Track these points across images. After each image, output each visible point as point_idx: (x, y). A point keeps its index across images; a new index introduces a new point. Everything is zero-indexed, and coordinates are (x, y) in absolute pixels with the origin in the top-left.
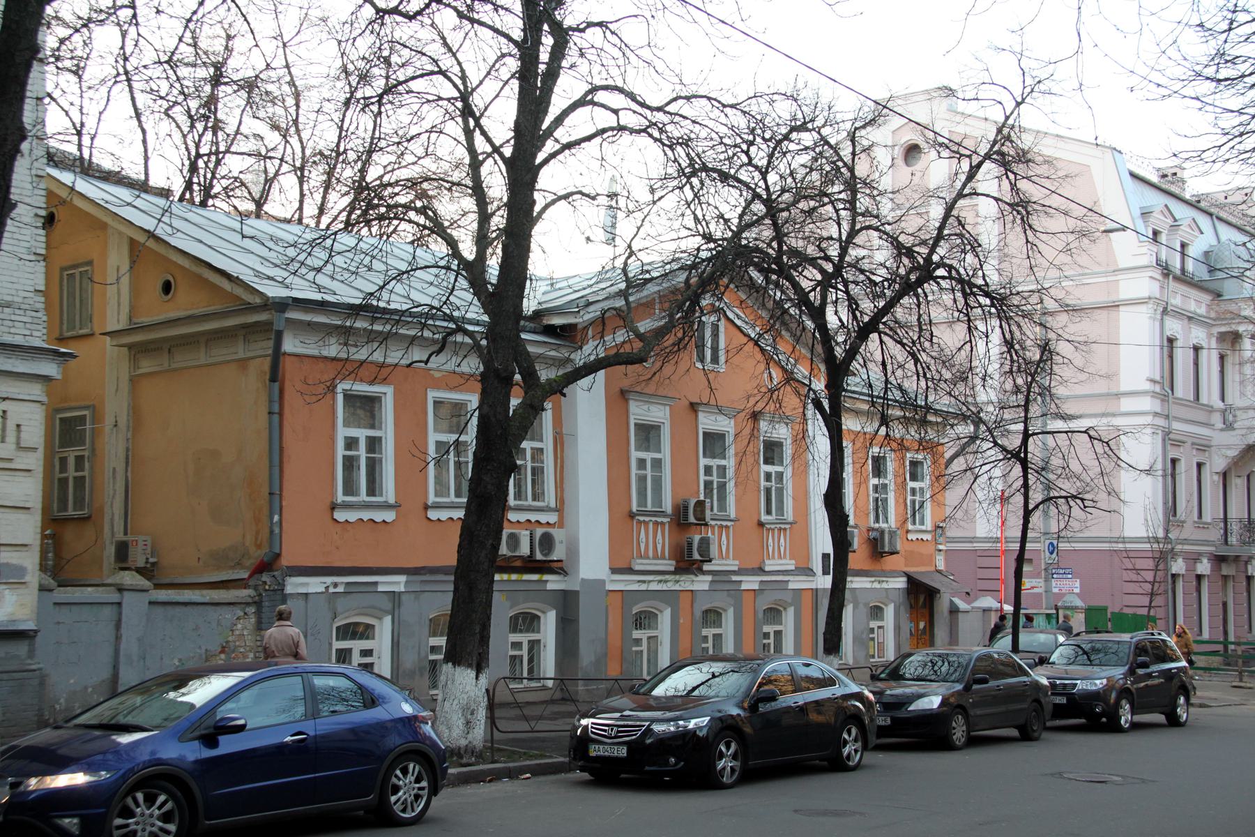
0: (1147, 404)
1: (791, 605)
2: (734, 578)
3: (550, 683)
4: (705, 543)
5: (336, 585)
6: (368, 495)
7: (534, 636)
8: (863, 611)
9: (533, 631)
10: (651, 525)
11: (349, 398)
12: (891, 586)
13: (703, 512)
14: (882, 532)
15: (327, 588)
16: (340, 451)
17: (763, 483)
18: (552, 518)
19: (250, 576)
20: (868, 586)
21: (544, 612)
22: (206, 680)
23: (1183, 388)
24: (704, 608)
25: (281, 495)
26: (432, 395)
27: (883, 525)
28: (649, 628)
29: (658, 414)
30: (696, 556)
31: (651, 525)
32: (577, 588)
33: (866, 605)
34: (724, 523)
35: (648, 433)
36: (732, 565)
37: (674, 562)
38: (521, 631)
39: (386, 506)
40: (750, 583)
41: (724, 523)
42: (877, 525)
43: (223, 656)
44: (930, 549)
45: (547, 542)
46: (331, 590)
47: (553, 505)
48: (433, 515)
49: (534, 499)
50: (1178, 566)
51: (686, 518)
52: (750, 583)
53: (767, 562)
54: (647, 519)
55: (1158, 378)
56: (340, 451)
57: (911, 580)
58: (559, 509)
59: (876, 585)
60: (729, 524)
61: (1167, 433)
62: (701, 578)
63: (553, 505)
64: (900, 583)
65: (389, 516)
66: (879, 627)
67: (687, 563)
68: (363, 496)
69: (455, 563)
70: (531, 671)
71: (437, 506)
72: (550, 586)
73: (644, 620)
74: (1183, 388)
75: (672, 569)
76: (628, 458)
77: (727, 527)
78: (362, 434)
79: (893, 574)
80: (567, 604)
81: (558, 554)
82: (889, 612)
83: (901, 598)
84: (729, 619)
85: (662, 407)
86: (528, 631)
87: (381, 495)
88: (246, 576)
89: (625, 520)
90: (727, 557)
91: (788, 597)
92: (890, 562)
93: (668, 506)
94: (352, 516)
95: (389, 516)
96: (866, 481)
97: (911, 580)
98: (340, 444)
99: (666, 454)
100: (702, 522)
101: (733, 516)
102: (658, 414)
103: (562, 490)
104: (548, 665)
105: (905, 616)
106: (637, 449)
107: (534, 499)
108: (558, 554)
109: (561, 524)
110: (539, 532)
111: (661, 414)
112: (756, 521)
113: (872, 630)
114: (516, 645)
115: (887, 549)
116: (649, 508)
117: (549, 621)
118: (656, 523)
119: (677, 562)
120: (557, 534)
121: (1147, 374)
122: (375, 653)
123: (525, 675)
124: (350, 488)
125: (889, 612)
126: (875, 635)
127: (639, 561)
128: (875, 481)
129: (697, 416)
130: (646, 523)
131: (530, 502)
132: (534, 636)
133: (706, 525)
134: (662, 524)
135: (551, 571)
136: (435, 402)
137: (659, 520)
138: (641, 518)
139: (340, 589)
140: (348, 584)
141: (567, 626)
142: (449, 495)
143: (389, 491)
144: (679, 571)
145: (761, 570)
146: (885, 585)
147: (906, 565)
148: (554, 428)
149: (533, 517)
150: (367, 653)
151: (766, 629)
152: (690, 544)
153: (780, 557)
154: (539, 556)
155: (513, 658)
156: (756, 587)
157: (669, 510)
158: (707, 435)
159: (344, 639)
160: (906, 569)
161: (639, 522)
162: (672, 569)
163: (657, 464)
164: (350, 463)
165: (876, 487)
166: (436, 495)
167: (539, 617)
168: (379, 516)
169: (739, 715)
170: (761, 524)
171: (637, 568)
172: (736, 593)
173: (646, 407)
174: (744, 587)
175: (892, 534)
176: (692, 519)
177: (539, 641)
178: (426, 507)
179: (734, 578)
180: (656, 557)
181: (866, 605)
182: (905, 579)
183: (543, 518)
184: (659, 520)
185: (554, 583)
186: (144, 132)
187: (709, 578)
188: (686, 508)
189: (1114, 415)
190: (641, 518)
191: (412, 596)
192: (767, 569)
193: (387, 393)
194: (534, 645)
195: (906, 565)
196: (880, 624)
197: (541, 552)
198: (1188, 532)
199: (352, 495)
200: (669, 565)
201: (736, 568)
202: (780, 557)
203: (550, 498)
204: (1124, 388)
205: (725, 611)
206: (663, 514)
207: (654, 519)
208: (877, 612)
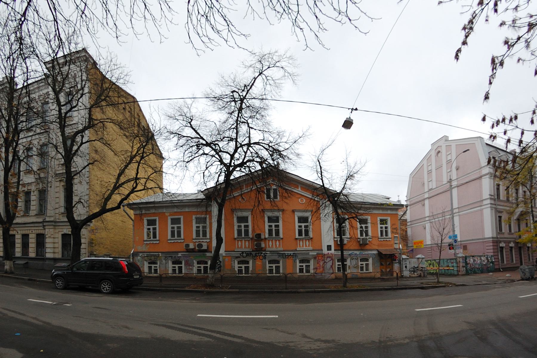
0: (489, 201)
23: (503, 196)
39: (207, 239)
44: (392, 243)
50: (502, 245)
55: (493, 194)
61: (496, 209)
71: (146, 241)
74: (503, 196)
82: (371, 261)
91: (310, 257)
95: (183, 241)
121: (489, 193)
131: (385, 237)
160: (377, 248)
164: (382, 232)
189: (482, 206)
193: (182, 217)
198: (506, 235)
203: (208, 236)
204: (484, 198)
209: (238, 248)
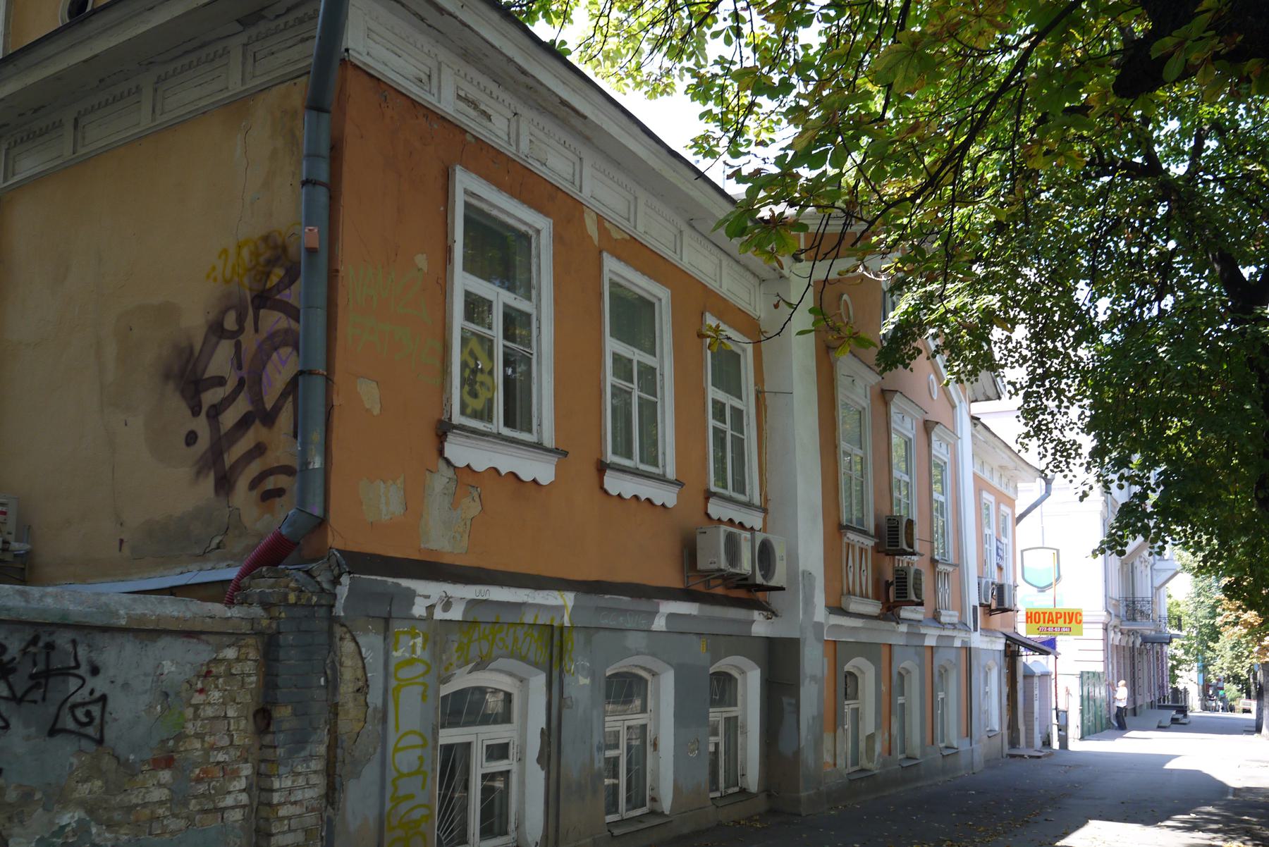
19: (246, 573)
25: (329, 379)
43: (165, 776)
46: (439, 615)
49: (616, 746)
68: (498, 425)
78: (498, 296)
88: (232, 573)
89: (837, 529)
107: (616, 746)
117: (751, 683)
122: (512, 751)
139: (456, 614)
150: (499, 751)
157: (870, 525)
169: (1125, 685)
178: (602, 467)
185: (761, 626)
186: (363, 659)
203: (754, 493)
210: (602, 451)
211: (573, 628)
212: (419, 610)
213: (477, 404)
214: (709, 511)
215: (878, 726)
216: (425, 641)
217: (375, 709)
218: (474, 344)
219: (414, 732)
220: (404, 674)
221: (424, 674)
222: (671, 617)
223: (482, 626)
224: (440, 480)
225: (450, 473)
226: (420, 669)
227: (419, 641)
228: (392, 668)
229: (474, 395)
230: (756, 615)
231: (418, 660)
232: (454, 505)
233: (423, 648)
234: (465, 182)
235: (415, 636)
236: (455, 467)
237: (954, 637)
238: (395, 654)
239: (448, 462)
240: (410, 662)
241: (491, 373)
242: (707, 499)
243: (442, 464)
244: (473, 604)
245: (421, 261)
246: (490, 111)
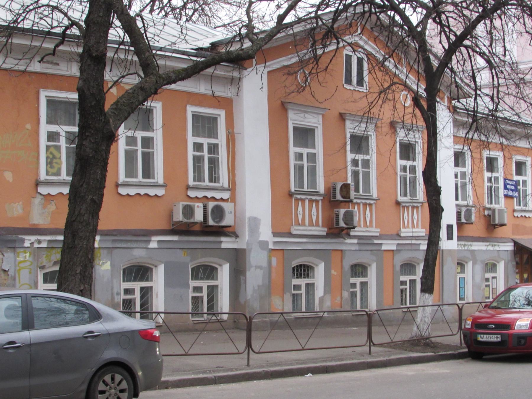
1: (470, 260)
2: (376, 241)
3: (225, 317)
4: (349, 216)
5: (39, 242)
6: (144, 177)
7: (212, 283)
8: (479, 268)
9: (412, 275)
10: (410, 208)
11: (196, 117)
12: (502, 248)
13: (348, 192)
14: (494, 211)
15: (32, 244)
16: (191, 152)
17: (399, 173)
18: (226, 195)
20: (484, 248)
21: (221, 265)
22: (98, 310)
24: (355, 261)
26: (191, 109)
27: (494, 206)
28: (308, 276)
29: (312, 120)
30: (342, 224)
31: (410, 208)
32: (244, 247)
33: (482, 262)
34: (368, 202)
35: (304, 135)
36: (374, 231)
37: (326, 229)
38: (202, 279)
39: (156, 186)
40: (389, 245)
41: (368, 202)
42: (491, 206)
45: (219, 212)
46: (36, 245)
47: (226, 185)
48: (123, 191)
51: (338, 199)
52: (389, 245)
53: (403, 230)
54: (303, 197)
56: (292, 162)
57: (516, 244)
58: (232, 188)
59: (490, 248)
60: (372, 202)
62: (349, 241)
63: (226, 185)
64: (509, 247)
65: (160, 192)
66: (493, 278)
67: (338, 230)
69: (64, 227)
70: (211, 307)
71: (126, 185)
72: (224, 246)
73: (303, 270)
75: (325, 234)
76: (288, 152)
77: (370, 205)
78: (205, 141)
79: (503, 240)
80: (238, 260)
81: (228, 220)
82: (501, 267)
83: (509, 257)
84: (372, 272)
85: (316, 116)
86: (208, 278)
87: (154, 178)
89: (284, 199)
90: (371, 226)
92: (500, 232)
93: (321, 188)
94: (132, 191)
96: (481, 172)
97: (516, 244)
98: (190, 147)
99: (319, 149)
100: (347, 200)
101: (375, 196)
102: (312, 120)
103: (234, 176)
104: (224, 303)
105: (512, 268)
106: (295, 146)
108: (228, 220)
109: (233, 199)
110: (211, 205)
111: (315, 120)
112: (394, 201)
113: (487, 280)
114: (198, 289)
115: (497, 222)
116: (306, 189)
117: (224, 273)
118: (311, 201)
119: (330, 229)
120: (227, 207)
123: (205, 310)
124: (198, 177)
125: (501, 267)
126: (490, 283)
127: (296, 228)
128: (489, 174)
129: (345, 125)
130: (303, 201)
131: (207, 183)
132: (212, 283)
133: (351, 201)
134: (317, 201)
135: (226, 235)
136: (193, 115)
137: (314, 198)
138: (299, 197)
139: (44, 245)
140: (398, 244)
141: (238, 274)
142: (136, 177)
143: (159, 176)
144: (329, 235)
145: (398, 236)
146: (497, 248)
147: (513, 233)
148: (227, 129)
149: (209, 194)
151: (403, 278)
152: (338, 216)
153: (413, 226)
154: (211, 222)
155: (402, 291)
156: (394, 248)
158: (353, 137)
159: (129, 280)
161: (297, 200)
162: (325, 234)
163: (312, 158)
164: (198, 160)
165: (490, 180)
166: (127, 176)
167: (217, 269)
168: (152, 192)
170: (398, 203)
171: (295, 232)
172: (378, 251)
173: (302, 115)
174: (384, 248)
175: (500, 211)
176: (339, 197)
177: (217, 286)
179: (376, 241)
180: (311, 224)
181: (482, 262)
182: (512, 244)
183: (218, 195)
184: (314, 198)
185: (227, 243)
187: (355, 241)
188: (335, 189)
190: (299, 197)
191: (105, 251)
192: (402, 235)
194: (364, 285)
195: (513, 233)
196: (493, 275)
197: (214, 219)
199: (149, 177)
200: (322, 231)
201: (378, 234)
202: (413, 226)
203: (224, 180)
205: (370, 265)
206: (317, 193)
207: (309, 197)
208: (491, 267)
209: (298, 224)
210: (38, 174)
211: (99, 248)
212: (27, 244)
213: (54, 170)
214: (119, 192)
215: (325, 292)
216: (30, 254)
217: (12, 276)
218: (52, 150)
219: (26, 284)
220: (22, 265)
221: (30, 265)
222: (159, 242)
223: (57, 249)
224: (38, 200)
225: (42, 197)
226: (28, 263)
227: (28, 255)
228: (17, 263)
229: (52, 167)
230: (223, 239)
231: (27, 261)
232: (44, 207)
233: (30, 256)
234: (191, 109)
235: (26, 253)
236: (44, 195)
237: (381, 244)
238: (18, 259)
239: (41, 194)
240: (24, 261)
241: (60, 158)
242: (187, 189)
243: (38, 195)
244: (50, 241)
245: (28, 126)
246: (57, 62)
